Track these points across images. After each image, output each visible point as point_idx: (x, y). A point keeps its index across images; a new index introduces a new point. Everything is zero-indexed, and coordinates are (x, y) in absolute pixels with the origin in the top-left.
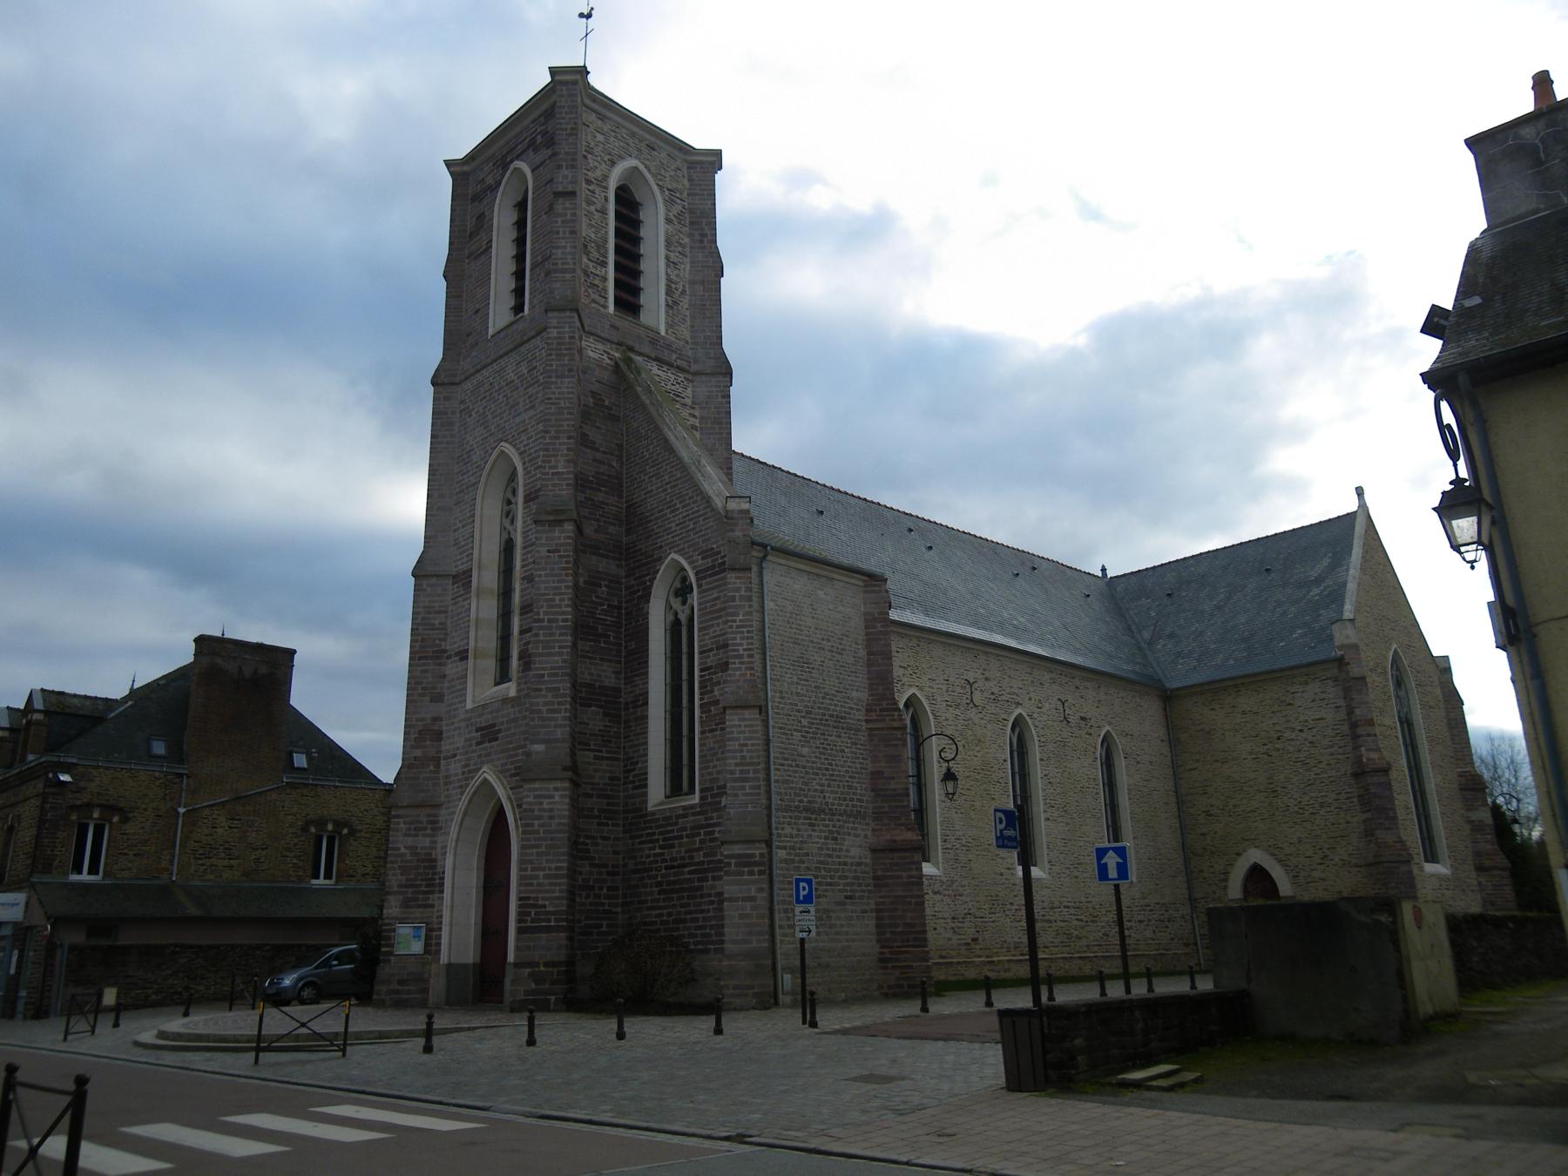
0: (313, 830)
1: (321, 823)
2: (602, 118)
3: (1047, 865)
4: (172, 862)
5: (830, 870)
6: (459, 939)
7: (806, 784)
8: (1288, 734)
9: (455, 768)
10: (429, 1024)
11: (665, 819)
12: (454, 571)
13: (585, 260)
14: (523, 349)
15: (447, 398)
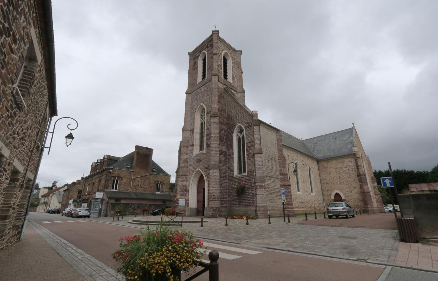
0: (156, 183)
1: (158, 182)
2: (221, 42)
3: (301, 192)
4: (130, 187)
5: (273, 189)
6: (193, 203)
7: (269, 171)
8: (343, 168)
9: (191, 168)
10: (202, 220)
11: (239, 178)
12: (190, 129)
13: (218, 68)
14: (205, 85)
15: (188, 96)
